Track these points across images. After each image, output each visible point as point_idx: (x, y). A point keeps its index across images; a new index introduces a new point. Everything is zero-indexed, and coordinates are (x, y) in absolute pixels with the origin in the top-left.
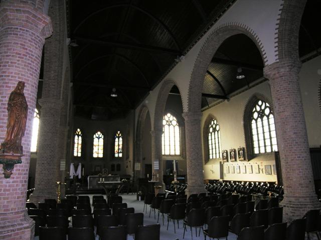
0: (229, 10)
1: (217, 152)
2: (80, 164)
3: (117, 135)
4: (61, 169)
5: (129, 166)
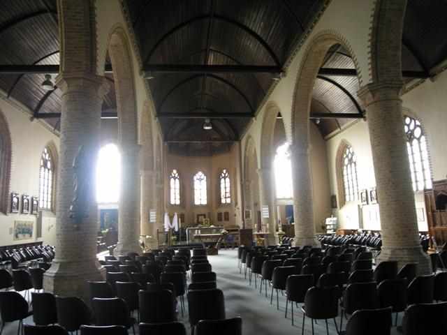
0: (317, 26)
1: (356, 192)
2: (176, 214)
3: (223, 175)
4: (151, 221)
5: (237, 215)
